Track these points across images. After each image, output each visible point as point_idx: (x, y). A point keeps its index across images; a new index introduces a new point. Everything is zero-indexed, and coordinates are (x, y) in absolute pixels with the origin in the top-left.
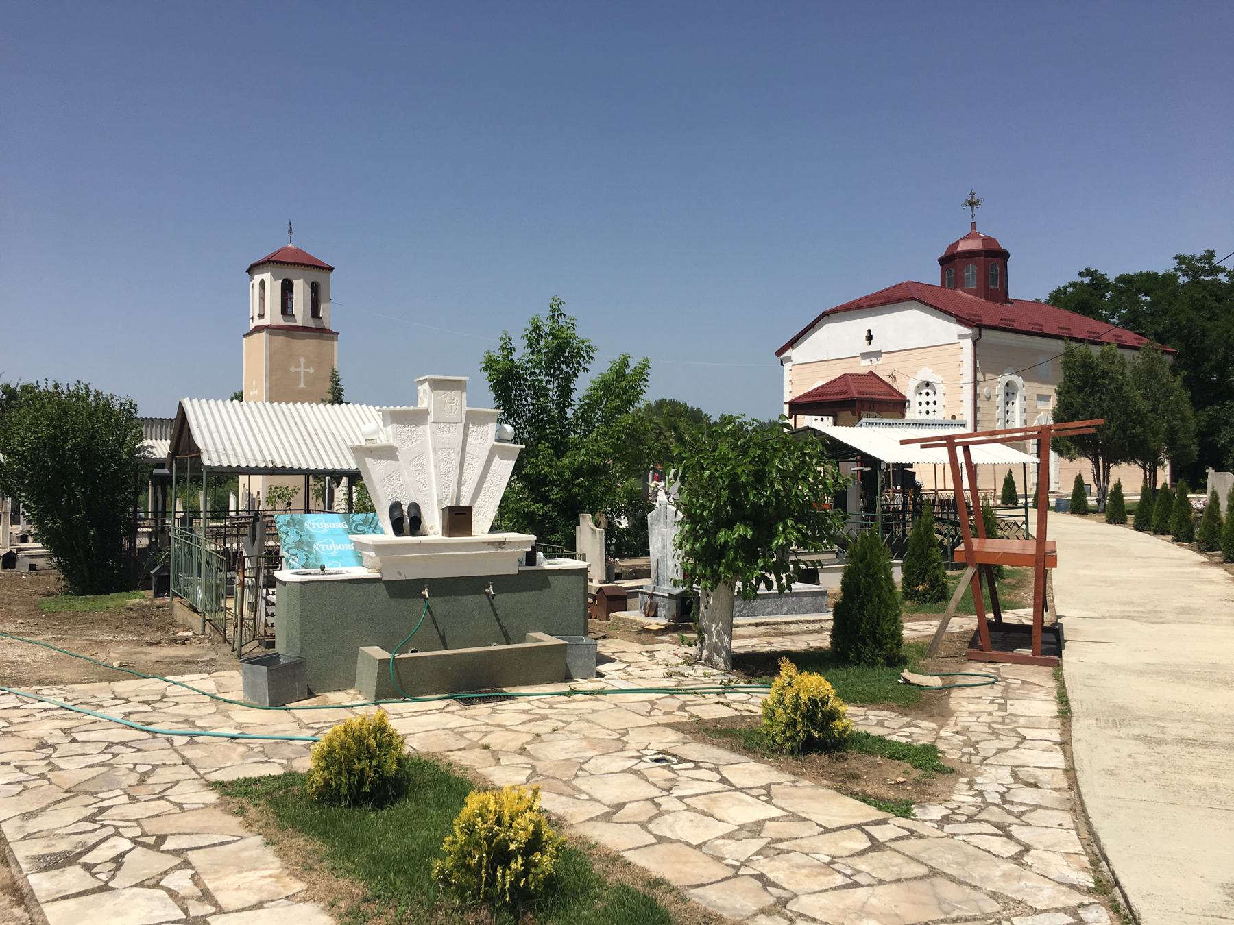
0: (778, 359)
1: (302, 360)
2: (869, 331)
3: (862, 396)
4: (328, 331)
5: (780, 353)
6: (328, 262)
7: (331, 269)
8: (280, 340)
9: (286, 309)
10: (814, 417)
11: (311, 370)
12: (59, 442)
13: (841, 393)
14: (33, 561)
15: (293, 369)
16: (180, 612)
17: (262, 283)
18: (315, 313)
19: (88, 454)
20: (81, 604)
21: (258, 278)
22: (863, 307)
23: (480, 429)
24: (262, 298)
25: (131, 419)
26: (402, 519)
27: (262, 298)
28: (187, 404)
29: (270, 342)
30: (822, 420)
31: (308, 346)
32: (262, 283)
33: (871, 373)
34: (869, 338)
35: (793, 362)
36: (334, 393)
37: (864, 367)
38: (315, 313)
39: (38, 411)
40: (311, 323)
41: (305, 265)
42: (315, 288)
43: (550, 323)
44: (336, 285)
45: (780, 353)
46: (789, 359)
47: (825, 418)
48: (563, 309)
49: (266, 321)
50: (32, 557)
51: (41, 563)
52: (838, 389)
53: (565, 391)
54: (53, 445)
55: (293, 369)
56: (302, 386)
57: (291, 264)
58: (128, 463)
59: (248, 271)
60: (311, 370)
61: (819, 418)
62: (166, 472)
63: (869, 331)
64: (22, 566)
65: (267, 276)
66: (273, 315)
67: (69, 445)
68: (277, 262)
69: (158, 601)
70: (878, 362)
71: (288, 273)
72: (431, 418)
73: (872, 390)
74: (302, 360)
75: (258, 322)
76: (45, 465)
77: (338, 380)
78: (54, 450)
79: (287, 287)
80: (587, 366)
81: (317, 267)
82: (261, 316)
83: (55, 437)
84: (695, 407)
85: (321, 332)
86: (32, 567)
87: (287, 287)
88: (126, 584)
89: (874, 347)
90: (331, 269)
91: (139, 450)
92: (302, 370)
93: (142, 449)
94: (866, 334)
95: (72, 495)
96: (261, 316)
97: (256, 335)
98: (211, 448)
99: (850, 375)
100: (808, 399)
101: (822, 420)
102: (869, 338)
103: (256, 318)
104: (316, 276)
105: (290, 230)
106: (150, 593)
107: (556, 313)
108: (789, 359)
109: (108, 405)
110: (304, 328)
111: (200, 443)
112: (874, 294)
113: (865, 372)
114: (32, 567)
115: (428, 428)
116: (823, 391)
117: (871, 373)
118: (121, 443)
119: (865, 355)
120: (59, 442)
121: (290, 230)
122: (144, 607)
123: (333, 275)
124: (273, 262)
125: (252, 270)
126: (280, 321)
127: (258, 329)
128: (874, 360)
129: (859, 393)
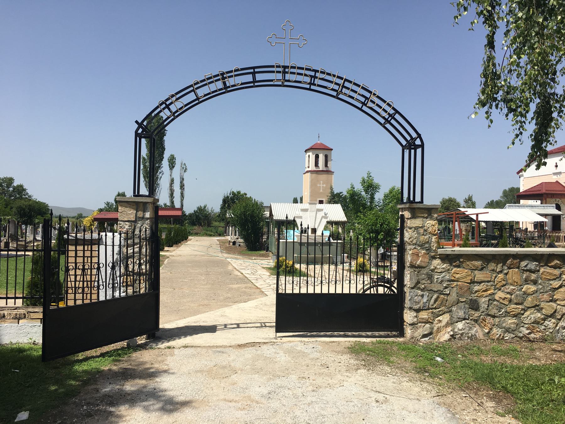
0: (518, 176)
1: (322, 182)
2: (556, 163)
3: (547, 192)
4: (330, 171)
5: (518, 173)
6: (331, 147)
7: (332, 149)
8: (314, 175)
9: (316, 164)
10: (533, 201)
11: (325, 185)
12: (245, 213)
13: (538, 191)
14: (240, 244)
15: (318, 185)
16: (271, 254)
17: (309, 156)
18: (326, 165)
19: (252, 216)
20: (250, 252)
21: (308, 154)
22: (553, 153)
23: (320, 212)
24: (309, 161)
25: (262, 206)
26: (303, 231)
27: (309, 161)
28: (272, 204)
29: (311, 176)
30: (537, 202)
31: (324, 177)
32: (309, 156)
33: (557, 182)
34: (557, 166)
35: (524, 177)
36: (331, 193)
37: (554, 179)
38: (326, 165)
39: (241, 205)
40: (325, 169)
41: (323, 149)
42: (326, 157)
43: (367, 179)
44: (334, 155)
45: (518, 173)
46: (522, 176)
47: (537, 201)
48: (371, 175)
49: (310, 169)
50: (240, 242)
51: (242, 244)
52: (537, 189)
53: (372, 198)
54: (244, 213)
55: (318, 185)
56: (321, 191)
57: (318, 149)
58: (261, 218)
59: (305, 152)
60: (325, 185)
61: (535, 201)
62: (269, 220)
63: (556, 163)
64: (237, 245)
65: (310, 154)
66: (312, 167)
67: (248, 213)
68: (314, 149)
69: (267, 253)
70: (560, 177)
71: (317, 152)
72: (309, 210)
73: (557, 189)
74: (322, 182)
75: (307, 169)
76: (242, 218)
77: (333, 189)
78: (244, 215)
79: (317, 157)
80: (379, 191)
81: (328, 149)
82: (309, 167)
83: (245, 211)
84: (447, 198)
85: (328, 172)
86: (239, 245)
87: (317, 157)
88: (260, 249)
89: (558, 170)
90: (332, 149)
91: (264, 215)
92: (321, 185)
93: (265, 214)
94: (555, 165)
95: (248, 226)
96: (309, 167)
97: (307, 174)
98: (276, 215)
99: (545, 183)
100: (524, 193)
101: (537, 202)
102: (557, 166)
103: (307, 168)
104: (326, 152)
105: (319, 137)
106: (265, 251)
107: (369, 176)
108: (522, 176)
109: (257, 203)
110: (322, 171)
111: (273, 214)
112: (561, 147)
113: (554, 181)
114: (239, 245)
115: (308, 212)
116: (533, 190)
117: (557, 182)
118: (259, 213)
119: (555, 174)
120: (245, 213)
121: (319, 137)
122: (263, 254)
123: (332, 151)
124: (312, 149)
125: (306, 151)
126: (314, 169)
127: (307, 172)
128: (558, 176)
129: (547, 191)
